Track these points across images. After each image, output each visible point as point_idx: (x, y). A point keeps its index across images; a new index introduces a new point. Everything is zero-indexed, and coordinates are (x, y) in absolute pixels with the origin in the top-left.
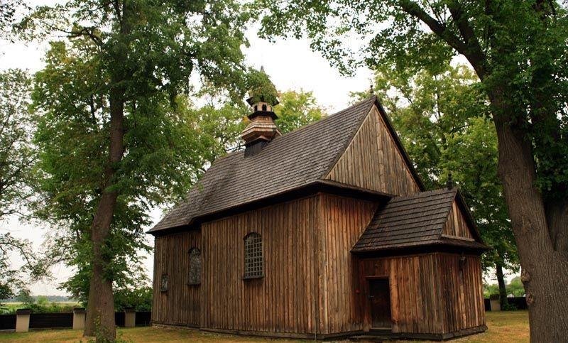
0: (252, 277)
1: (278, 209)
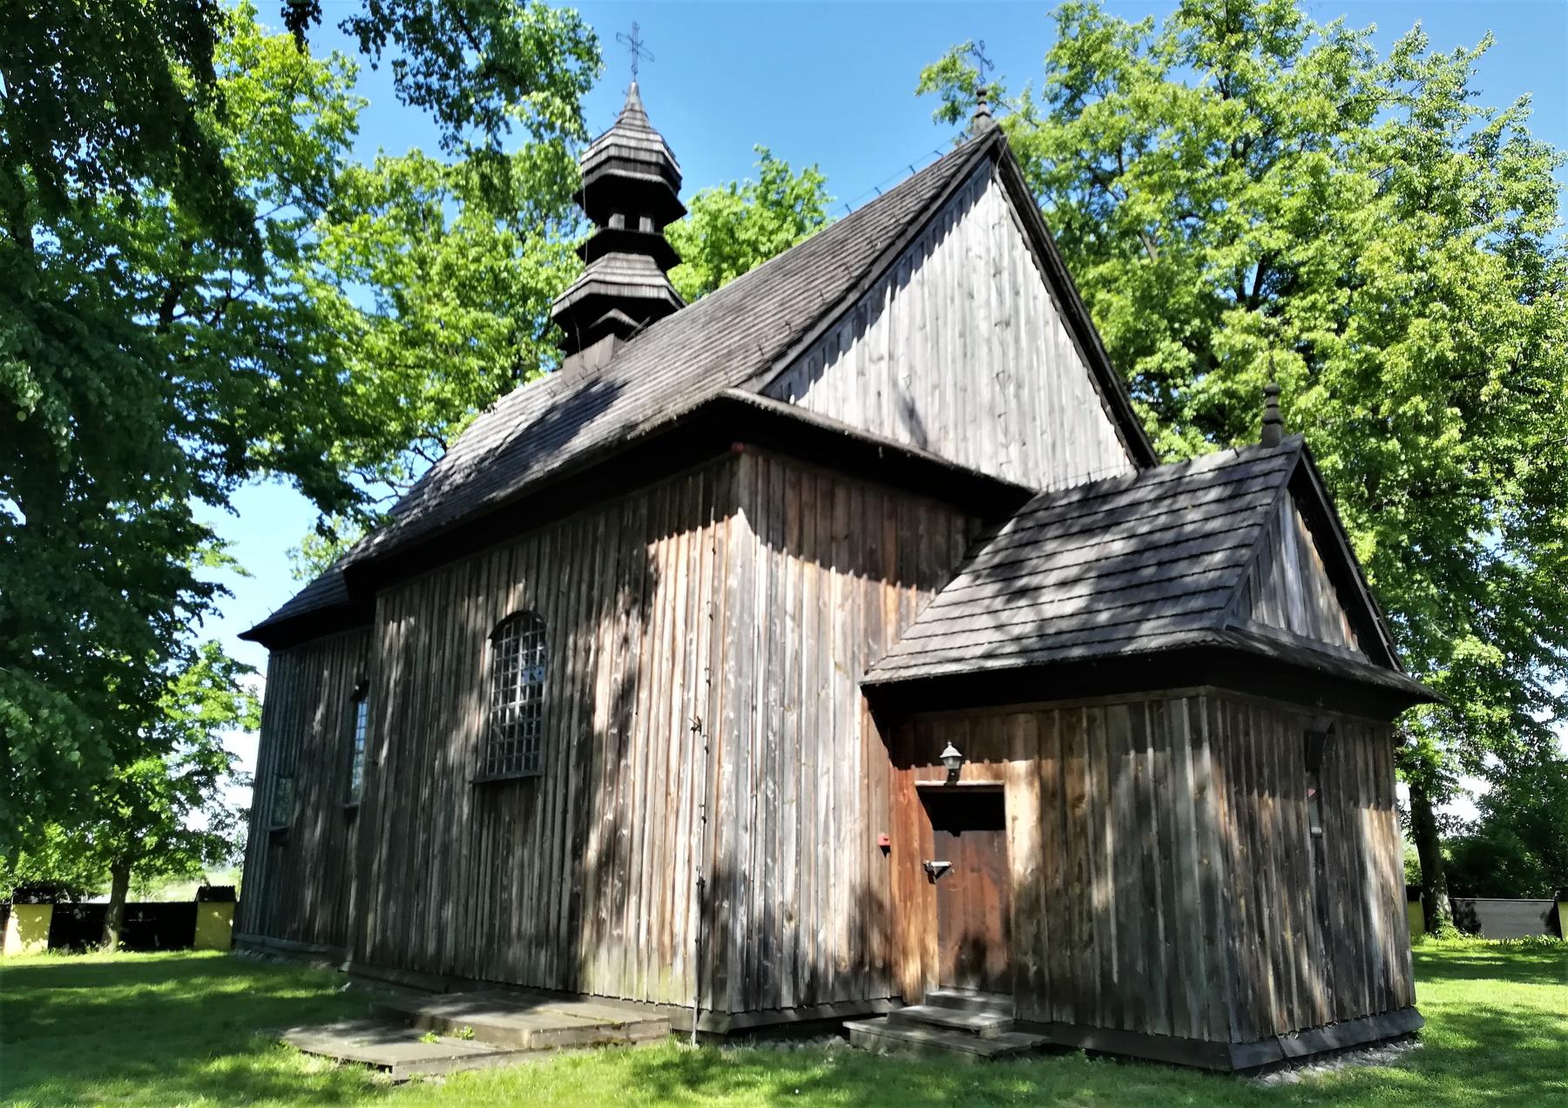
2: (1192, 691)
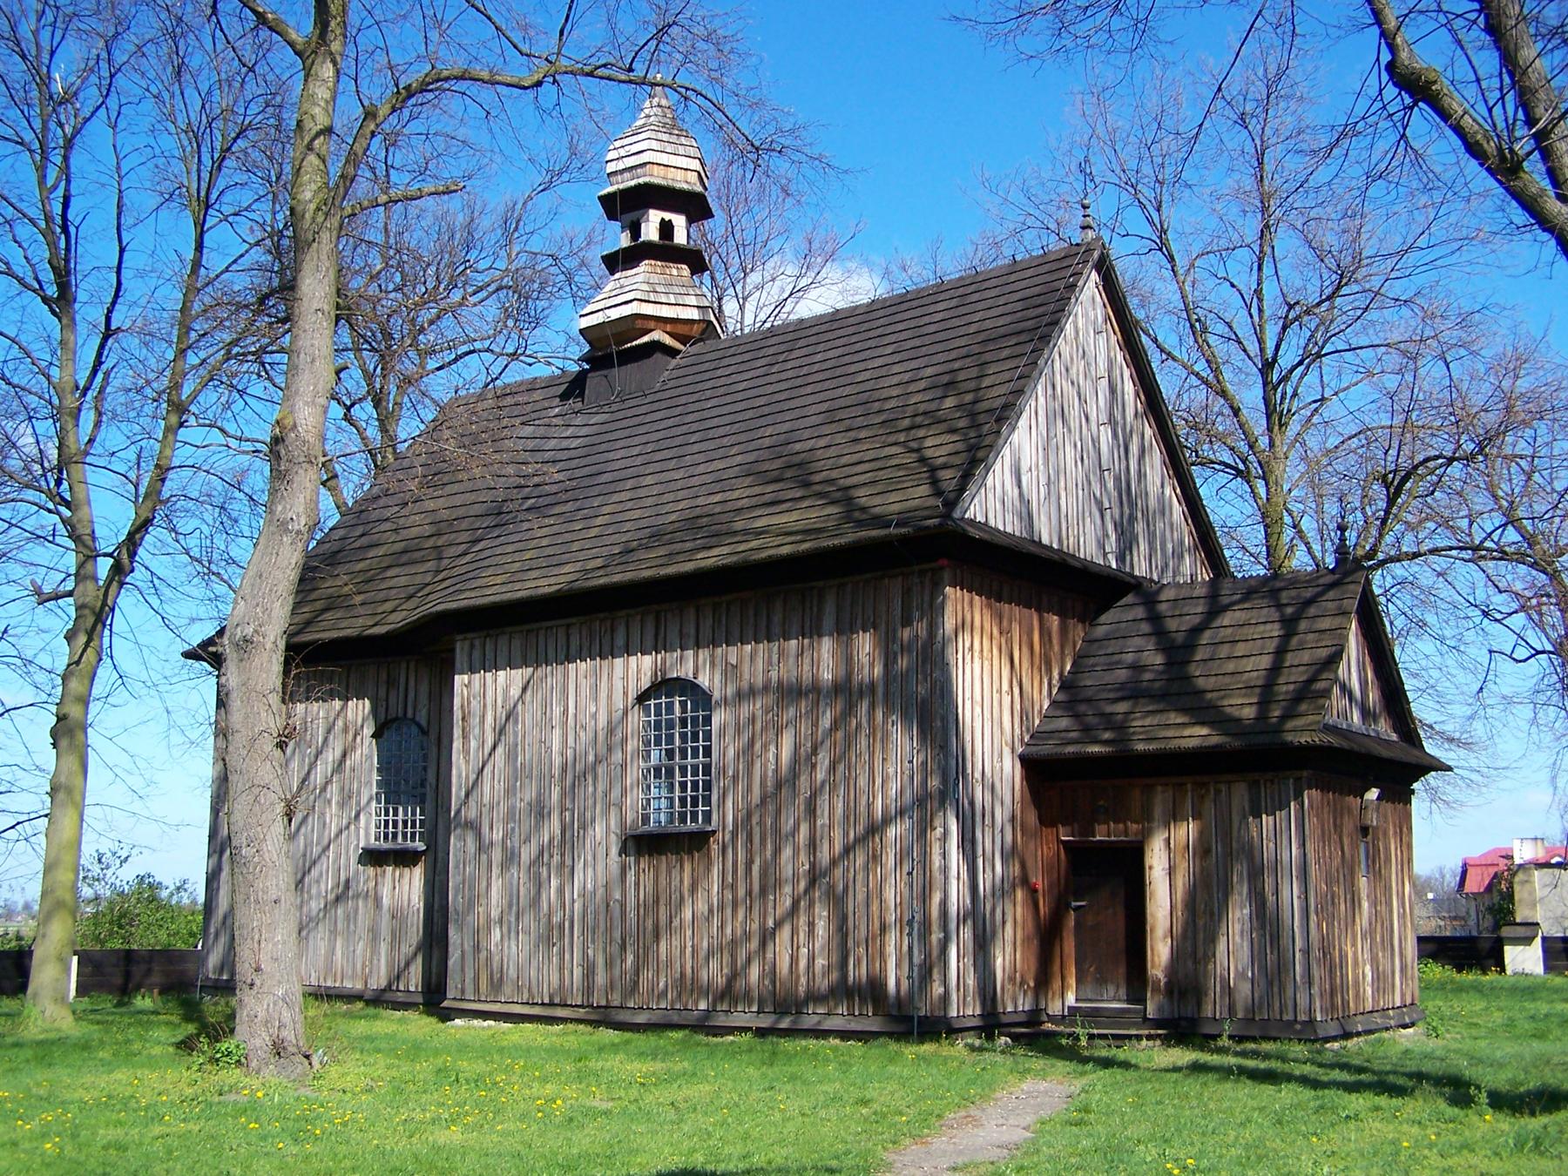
0: (683, 828)
1: (779, 605)
2: (1298, 774)
